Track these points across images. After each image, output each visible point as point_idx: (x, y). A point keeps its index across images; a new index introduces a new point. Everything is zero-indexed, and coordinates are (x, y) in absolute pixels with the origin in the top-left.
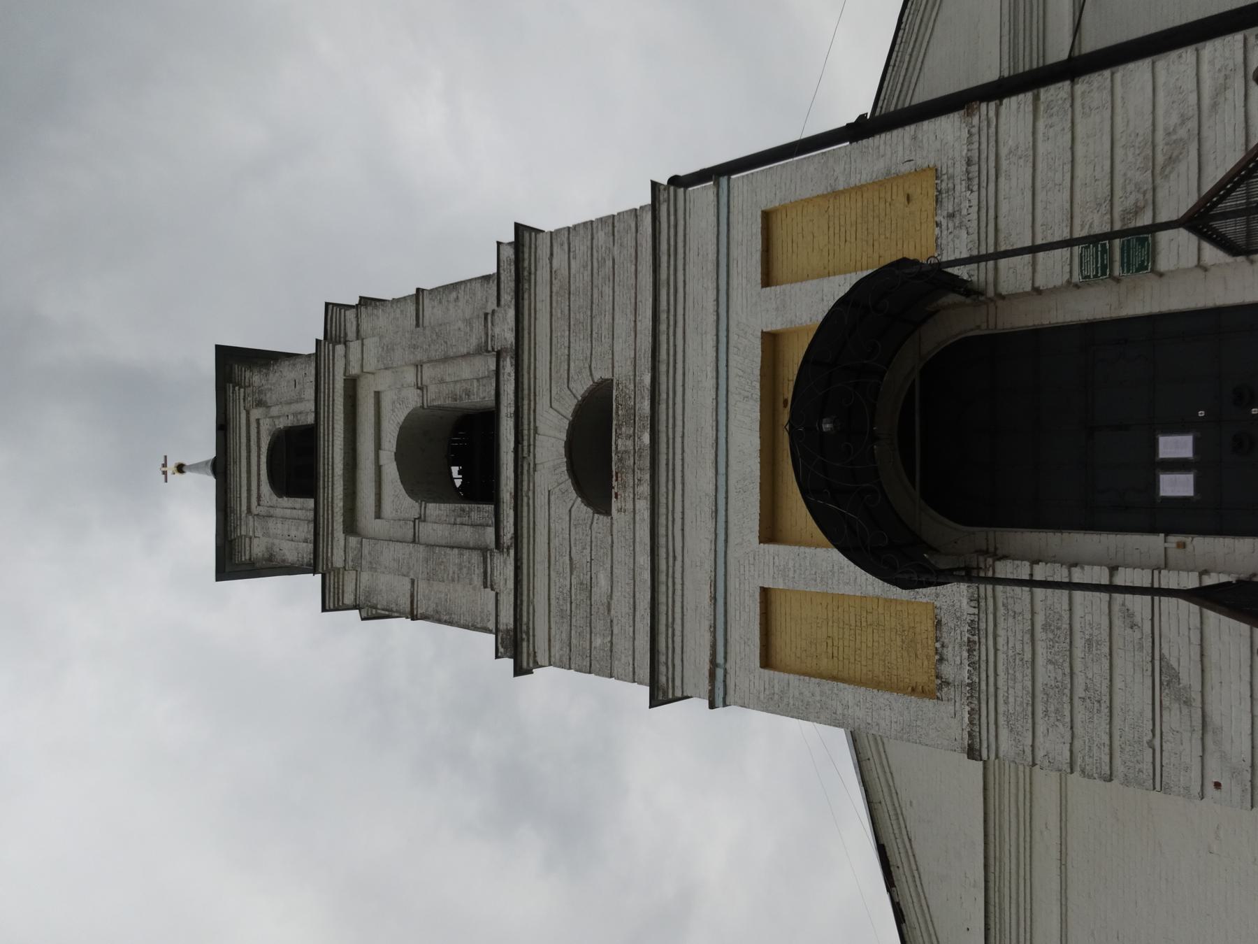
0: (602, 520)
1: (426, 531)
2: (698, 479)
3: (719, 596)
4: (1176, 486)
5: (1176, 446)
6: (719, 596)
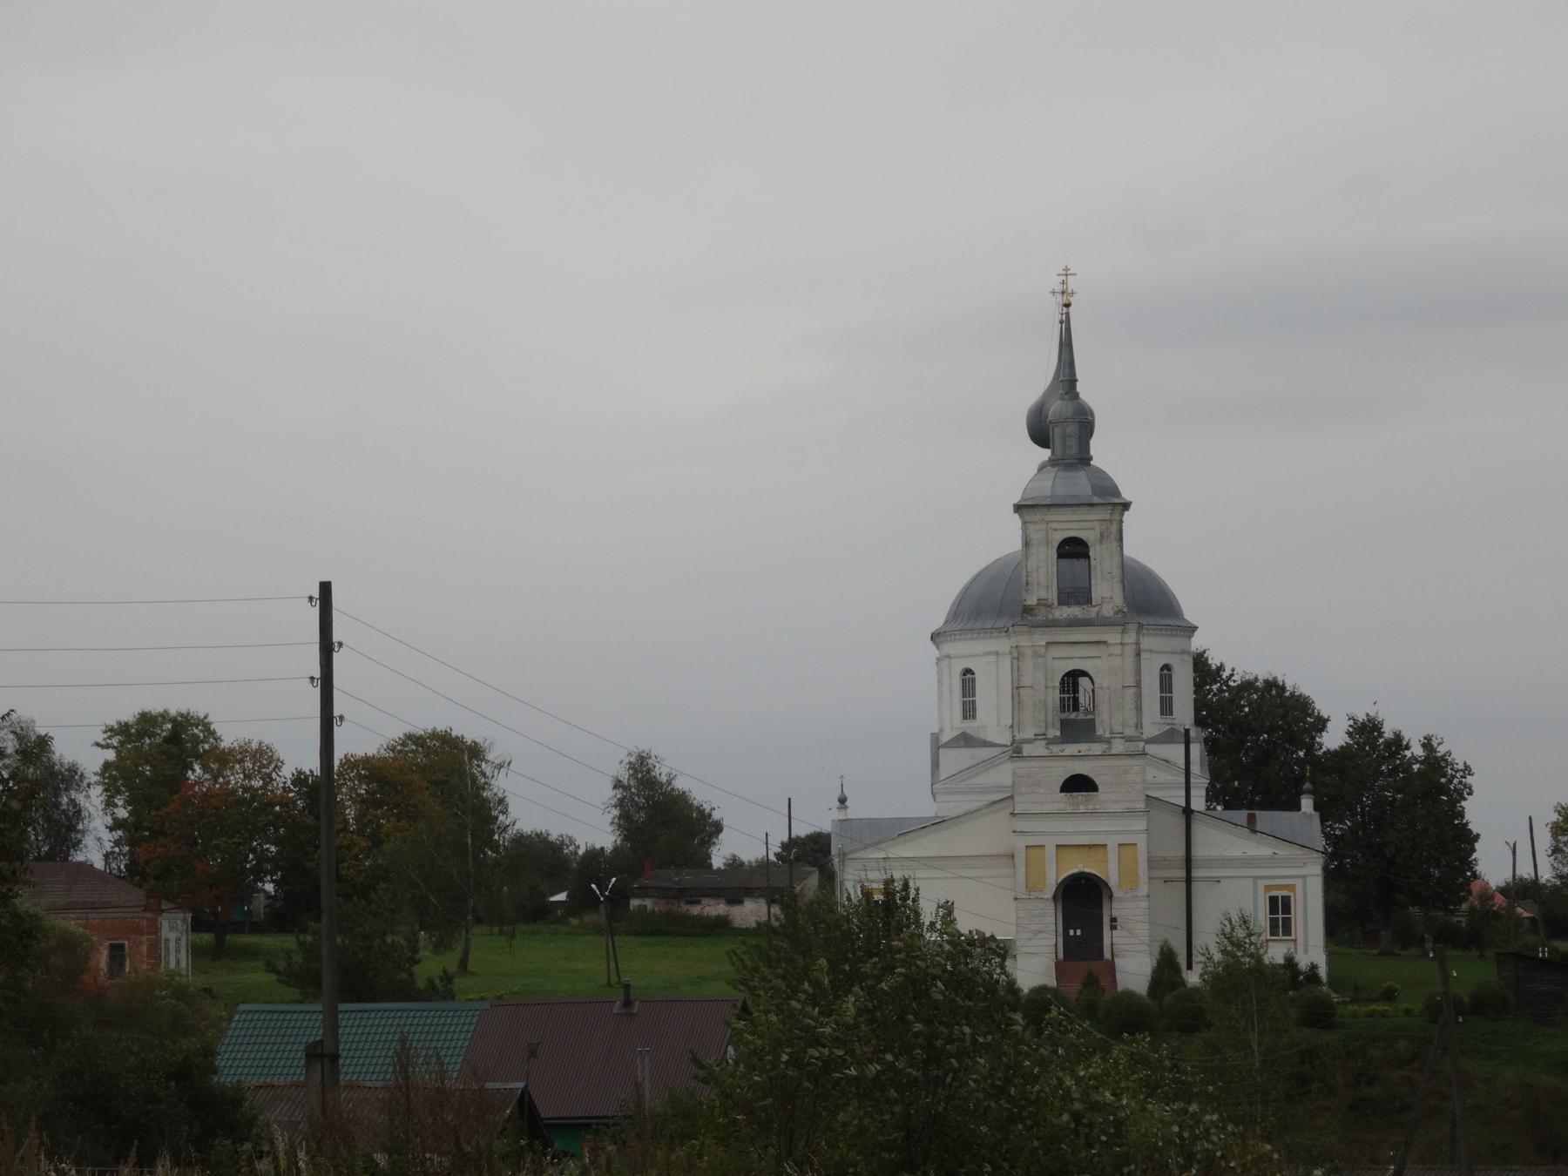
0: (1058, 789)
1: (1050, 691)
2: (1070, 825)
4: (1071, 932)
5: (1079, 932)
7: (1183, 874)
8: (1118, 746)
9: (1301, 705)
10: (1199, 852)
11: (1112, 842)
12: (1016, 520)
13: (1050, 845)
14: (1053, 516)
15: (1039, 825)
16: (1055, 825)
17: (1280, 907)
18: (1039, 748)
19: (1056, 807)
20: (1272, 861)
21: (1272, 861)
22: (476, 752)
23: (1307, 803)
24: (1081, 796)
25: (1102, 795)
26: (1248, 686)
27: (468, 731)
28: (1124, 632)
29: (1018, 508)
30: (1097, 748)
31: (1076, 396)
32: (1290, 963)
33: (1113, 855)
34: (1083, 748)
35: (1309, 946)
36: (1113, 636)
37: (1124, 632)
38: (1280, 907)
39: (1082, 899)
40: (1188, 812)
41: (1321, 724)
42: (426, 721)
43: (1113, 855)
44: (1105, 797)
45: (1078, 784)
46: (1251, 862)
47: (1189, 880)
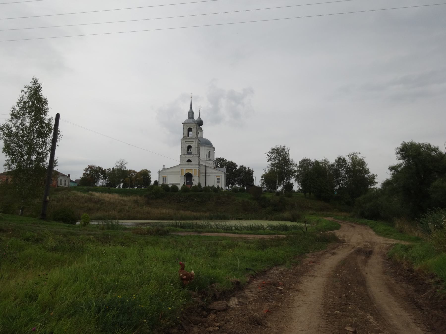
0: (37, 77)
2: (188, 166)
8: (195, 156)
9: (235, 164)
10: (207, 172)
11: (193, 169)
13: (185, 169)
14: (187, 125)
15: (184, 166)
16: (186, 166)
17: (218, 179)
18: (184, 156)
20: (217, 173)
21: (217, 173)
22: (150, 172)
23: (224, 167)
25: (192, 162)
26: (228, 162)
27: (149, 169)
30: (192, 156)
32: (218, 187)
33: (193, 171)
34: (190, 156)
35: (222, 185)
36: (194, 141)
38: (218, 179)
39: (189, 176)
40: (206, 166)
41: (237, 166)
42: (144, 168)
43: (193, 171)
45: (189, 161)
46: (215, 173)
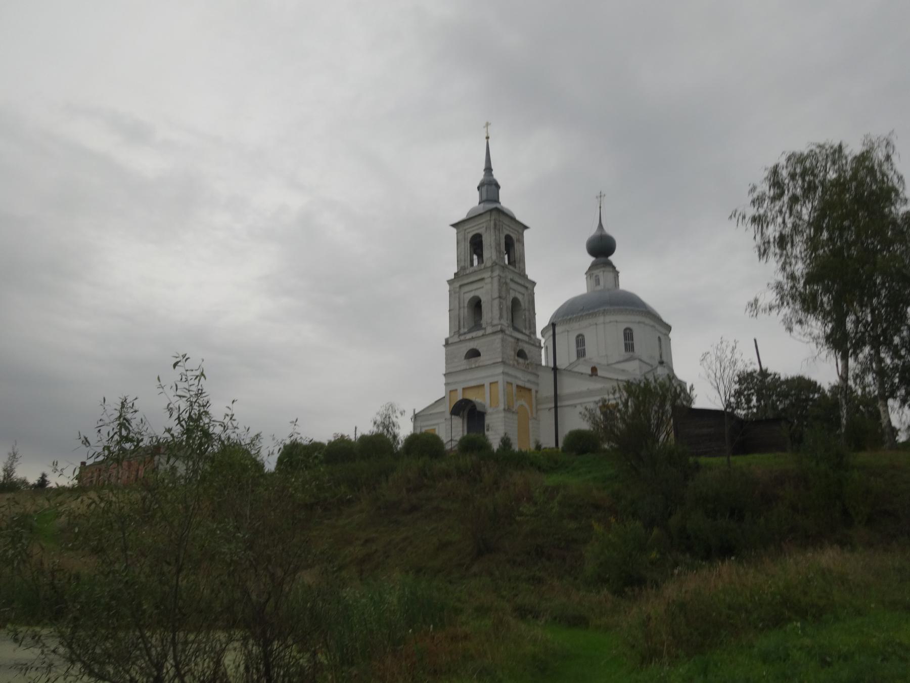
3: (456, 383)
6: (456, 383)
7: (553, 405)
12: (454, 231)
19: (463, 367)
24: (473, 360)
25: (482, 358)
26: (787, 381)
28: (492, 271)
29: (454, 225)
31: (492, 175)
37: (492, 271)
44: (484, 359)
47: (556, 407)
